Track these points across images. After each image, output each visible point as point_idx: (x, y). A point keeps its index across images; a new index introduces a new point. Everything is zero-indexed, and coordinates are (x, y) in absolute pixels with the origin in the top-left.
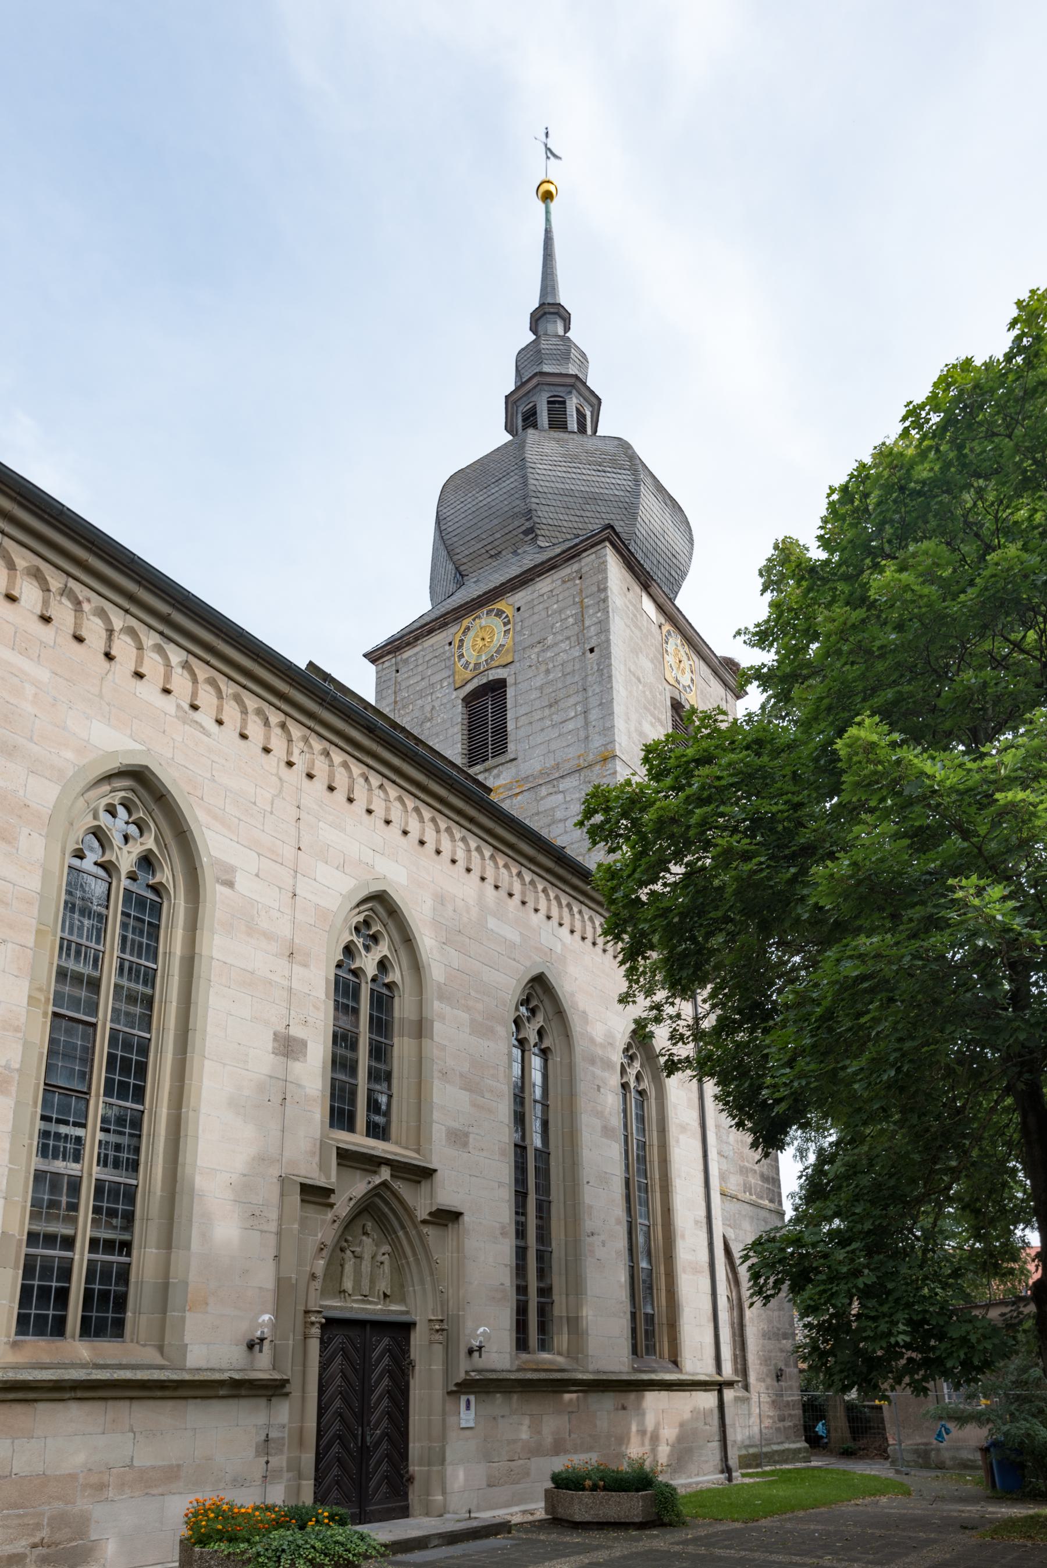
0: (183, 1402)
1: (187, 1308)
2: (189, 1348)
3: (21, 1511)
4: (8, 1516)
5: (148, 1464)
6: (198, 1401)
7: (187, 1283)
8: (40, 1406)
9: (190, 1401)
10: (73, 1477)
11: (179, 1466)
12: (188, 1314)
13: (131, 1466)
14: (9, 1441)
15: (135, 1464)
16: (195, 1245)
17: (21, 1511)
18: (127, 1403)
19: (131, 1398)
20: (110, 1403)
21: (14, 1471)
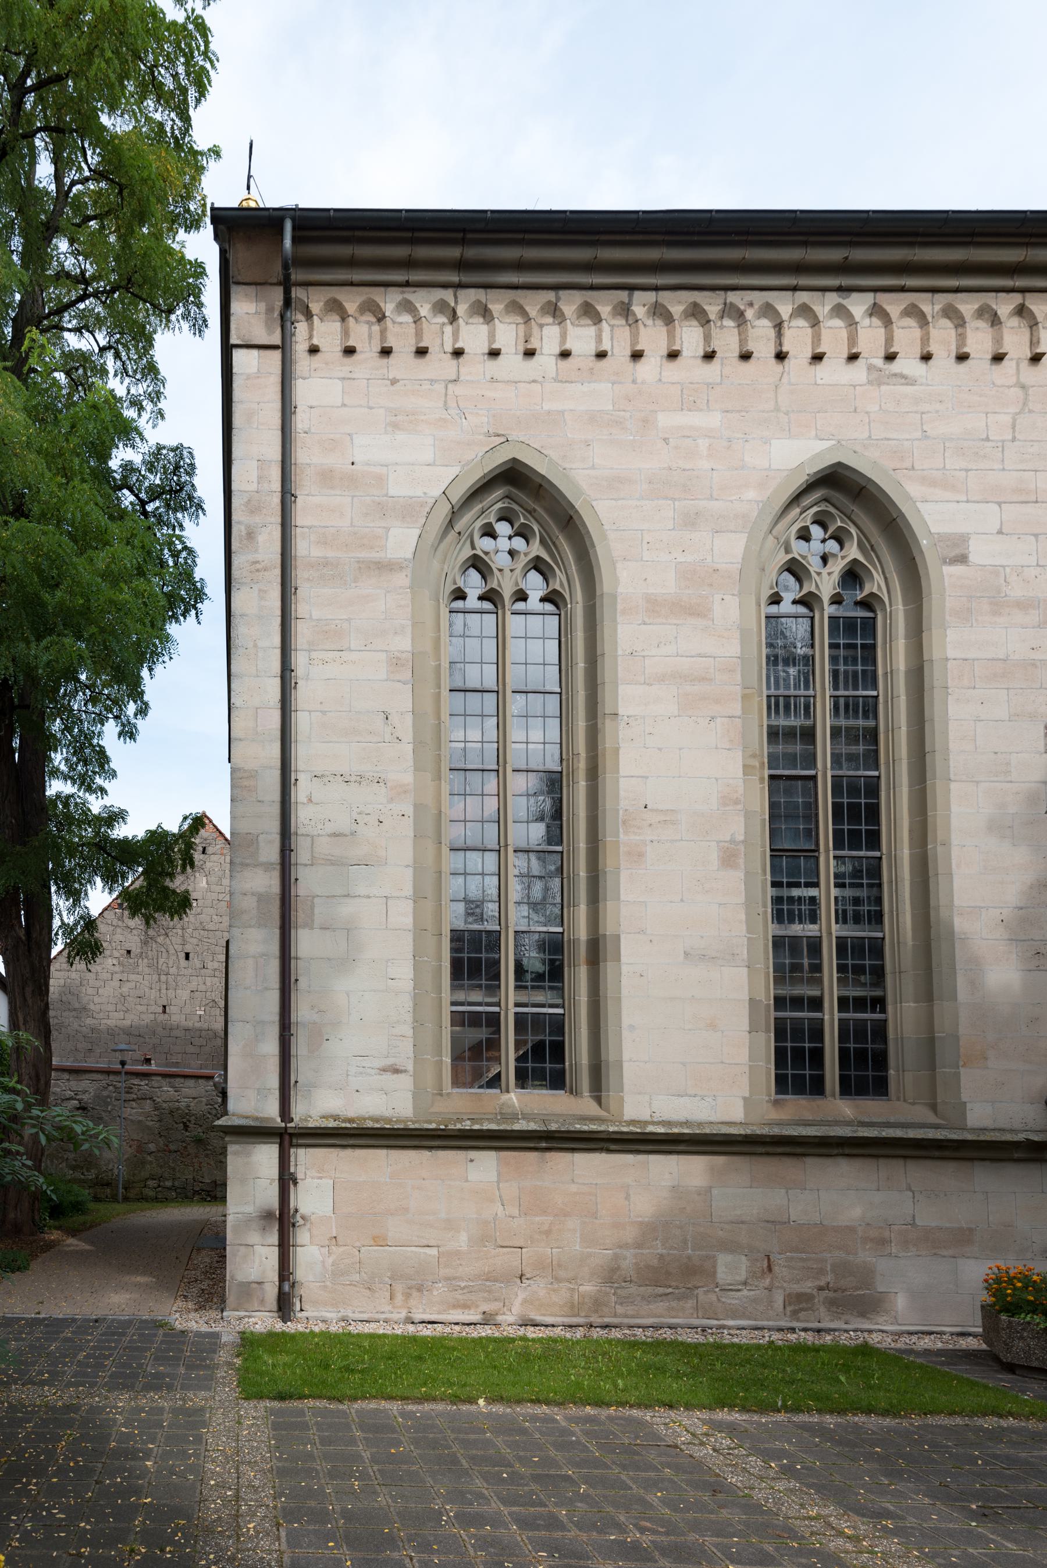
0: (939, 1163)
1: (961, 1063)
2: (969, 1106)
3: (804, 1255)
4: (792, 1258)
5: (933, 1224)
6: (987, 1163)
7: (957, 1038)
8: (809, 1160)
9: (976, 1163)
10: (851, 1229)
11: (971, 1230)
12: (962, 1070)
13: (913, 1224)
14: (783, 1191)
15: (918, 1222)
16: (963, 994)
17: (804, 1255)
18: (901, 1162)
19: (905, 1157)
20: (882, 1161)
21: (792, 1219)
